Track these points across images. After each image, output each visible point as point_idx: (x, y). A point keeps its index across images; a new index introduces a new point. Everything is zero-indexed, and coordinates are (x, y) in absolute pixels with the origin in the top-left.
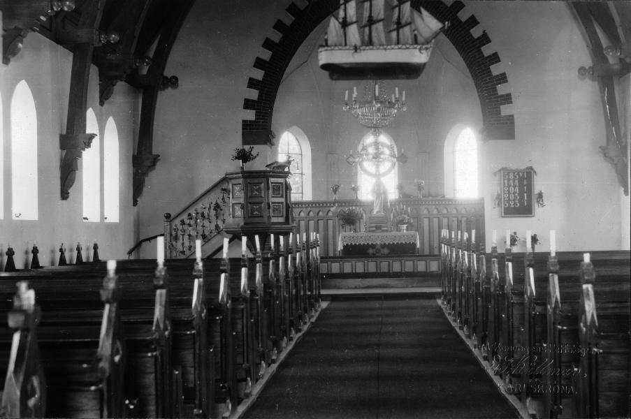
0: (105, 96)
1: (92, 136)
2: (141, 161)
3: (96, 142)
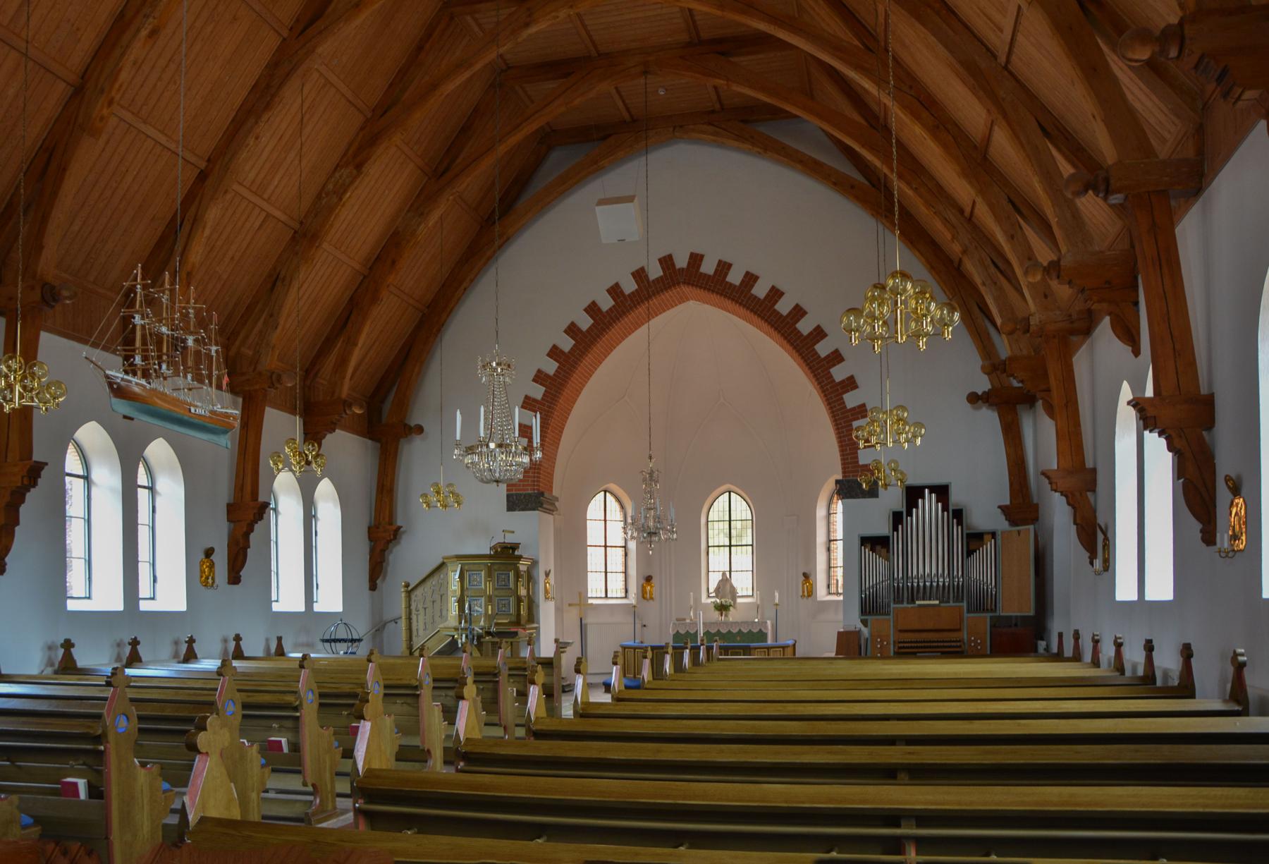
2: (377, 539)
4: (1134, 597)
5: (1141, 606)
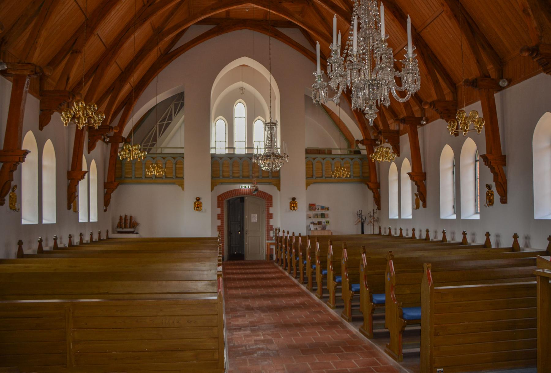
0: (44, 120)
1: (26, 152)
3: (32, 158)
5: (89, 224)
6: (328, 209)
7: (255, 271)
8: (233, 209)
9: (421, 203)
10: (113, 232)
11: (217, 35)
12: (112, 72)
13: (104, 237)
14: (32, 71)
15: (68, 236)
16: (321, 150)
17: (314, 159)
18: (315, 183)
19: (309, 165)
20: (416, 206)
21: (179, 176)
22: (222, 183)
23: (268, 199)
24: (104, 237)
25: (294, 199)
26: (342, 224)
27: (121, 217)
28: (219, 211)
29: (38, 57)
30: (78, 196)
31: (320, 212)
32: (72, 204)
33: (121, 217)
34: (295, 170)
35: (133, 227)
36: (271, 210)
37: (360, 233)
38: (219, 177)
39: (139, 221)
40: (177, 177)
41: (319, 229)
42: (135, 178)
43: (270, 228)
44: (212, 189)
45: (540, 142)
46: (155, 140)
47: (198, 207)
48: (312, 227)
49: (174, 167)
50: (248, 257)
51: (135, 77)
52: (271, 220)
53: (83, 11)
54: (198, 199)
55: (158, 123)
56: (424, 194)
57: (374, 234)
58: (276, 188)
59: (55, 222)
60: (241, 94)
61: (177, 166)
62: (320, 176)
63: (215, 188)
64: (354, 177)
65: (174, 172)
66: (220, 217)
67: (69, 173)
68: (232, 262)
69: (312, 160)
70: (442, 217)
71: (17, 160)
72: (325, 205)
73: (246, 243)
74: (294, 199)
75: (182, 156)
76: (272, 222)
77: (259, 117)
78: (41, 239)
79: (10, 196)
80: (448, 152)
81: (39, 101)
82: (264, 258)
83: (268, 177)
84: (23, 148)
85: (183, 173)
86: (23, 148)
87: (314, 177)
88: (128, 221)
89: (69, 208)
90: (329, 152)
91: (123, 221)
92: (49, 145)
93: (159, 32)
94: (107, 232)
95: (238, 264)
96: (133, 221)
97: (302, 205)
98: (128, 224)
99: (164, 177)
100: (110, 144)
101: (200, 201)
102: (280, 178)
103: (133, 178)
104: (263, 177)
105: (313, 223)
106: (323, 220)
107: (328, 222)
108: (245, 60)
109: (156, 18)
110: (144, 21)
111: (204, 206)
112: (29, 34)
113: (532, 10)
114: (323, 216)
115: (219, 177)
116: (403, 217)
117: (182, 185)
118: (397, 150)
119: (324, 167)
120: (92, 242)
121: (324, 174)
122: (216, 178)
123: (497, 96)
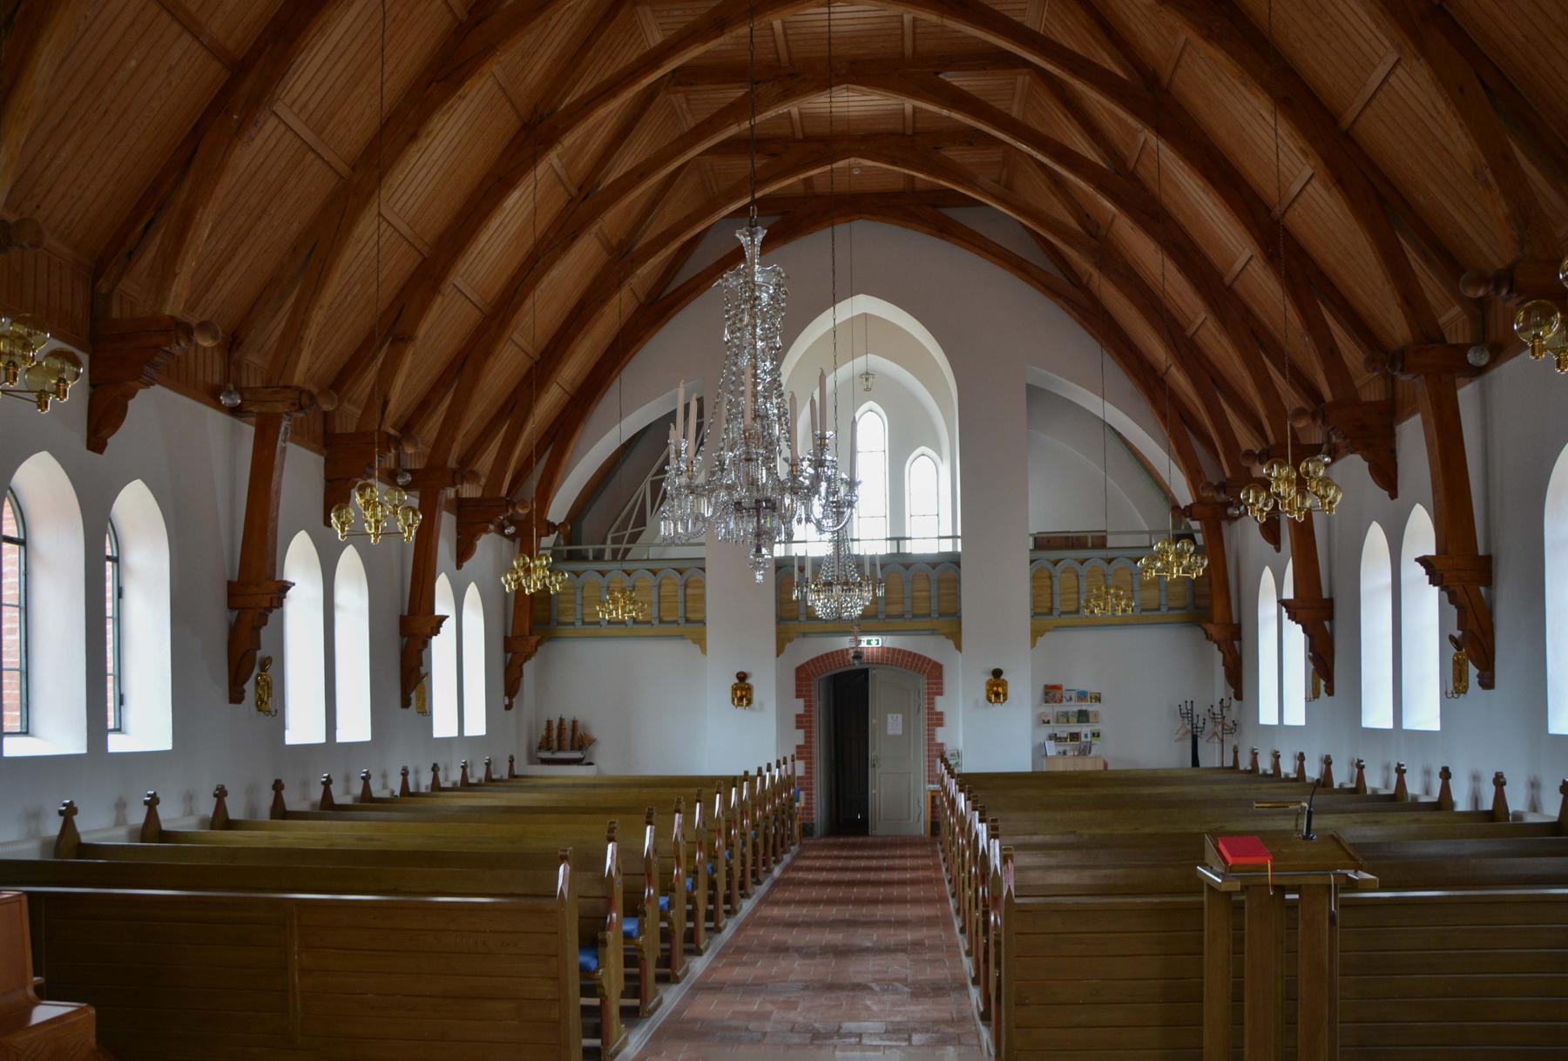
1: (443, 618)
3: (448, 627)
4: (319, 737)
6: (1098, 699)
7: (874, 863)
8: (841, 704)
9: (1473, 671)
10: (534, 760)
11: (785, 243)
12: (503, 368)
13: (501, 772)
14: (293, 404)
15: (400, 770)
16: (1078, 539)
17: (1056, 563)
18: (1057, 628)
19: (1041, 582)
20: (1455, 684)
21: (692, 616)
22: (805, 635)
23: (933, 674)
24: (501, 772)
25: (997, 673)
26: (1138, 738)
27: (549, 723)
28: (799, 706)
29: (305, 368)
30: (429, 674)
31: (1074, 707)
32: (413, 695)
33: (549, 723)
34: (1000, 598)
35: (580, 748)
36: (940, 704)
37: (1189, 764)
38: (797, 619)
39: (595, 732)
40: (687, 621)
41: (1070, 754)
42: (584, 623)
43: (939, 753)
44: (779, 651)
45: (1563, 524)
46: (641, 521)
47: (741, 699)
48: (1052, 749)
49: (680, 593)
50: (880, 826)
51: (572, 370)
52: (939, 730)
53: (411, 244)
54: (742, 677)
55: (649, 478)
56: (1330, 664)
57: (1222, 768)
58: (951, 643)
59: (368, 738)
60: (867, 384)
61: (689, 591)
62: (1073, 608)
63: (788, 646)
64: (1170, 609)
65: (681, 606)
66: (802, 722)
67: (403, 621)
68: (831, 840)
69: (1050, 566)
70: (1365, 724)
71: (267, 604)
72: (1091, 688)
73: (872, 791)
74: (997, 673)
75: (700, 565)
76: (941, 735)
77: (922, 449)
78: (153, 796)
79: (257, 683)
80: (1376, 537)
81: (322, 459)
82: (921, 828)
83: (929, 615)
84: (437, 613)
85: (703, 610)
86: (437, 613)
87: (1056, 613)
88: (568, 734)
89: (406, 703)
90: (1100, 542)
91: (555, 733)
92: (472, 594)
93: (621, 258)
94: (511, 761)
95: (854, 847)
96: (580, 732)
97: (1022, 688)
98: (566, 741)
99: (656, 622)
100: (518, 540)
101: (748, 681)
102: (959, 618)
103: (579, 624)
104: (915, 616)
105: (1054, 737)
106: (1084, 729)
107: (1096, 735)
108: (862, 304)
109: (612, 221)
110: (573, 240)
111: (757, 696)
112: (283, 324)
113: (1494, 172)
114: (1083, 716)
115: (797, 619)
116: (342, 737)
117: (700, 641)
118: (1386, 475)
119: (1083, 584)
120: (465, 785)
121: (1057, 604)
122: (791, 619)
123: (1467, 395)
